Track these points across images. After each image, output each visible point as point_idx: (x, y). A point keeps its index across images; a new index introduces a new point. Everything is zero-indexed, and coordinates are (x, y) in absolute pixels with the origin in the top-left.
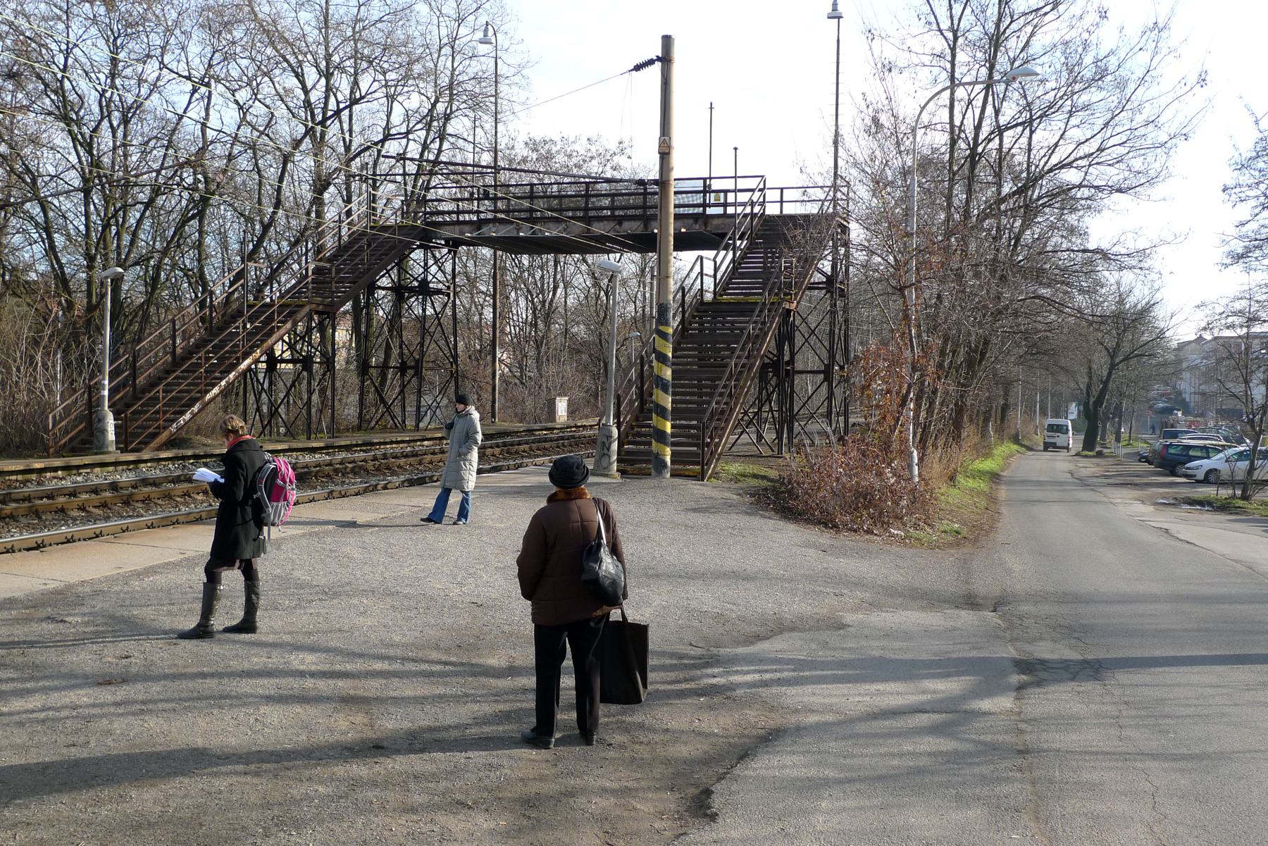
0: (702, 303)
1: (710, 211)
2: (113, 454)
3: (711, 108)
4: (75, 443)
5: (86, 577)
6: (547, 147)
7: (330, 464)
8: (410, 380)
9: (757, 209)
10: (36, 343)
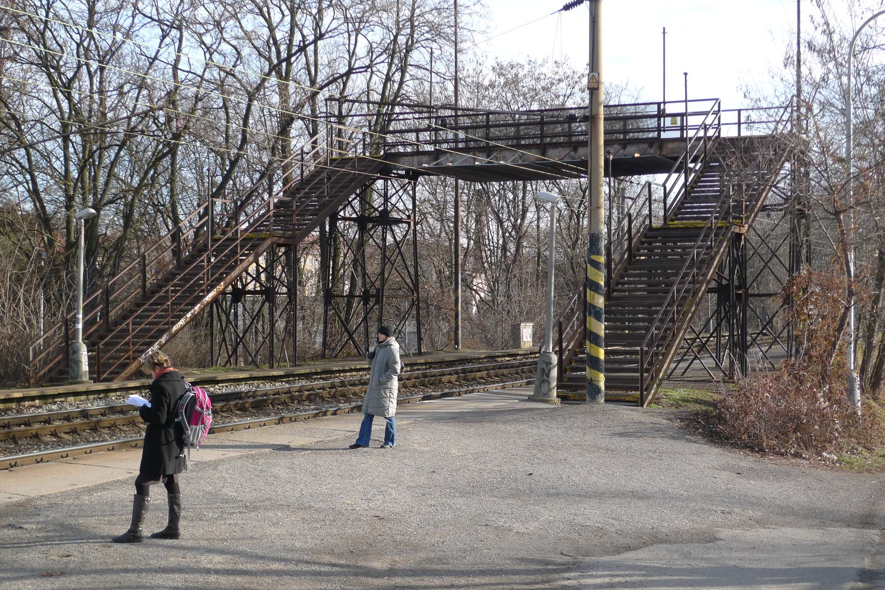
0: (650, 228)
1: (664, 135)
2: (86, 383)
3: (664, 33)
4: (53, 374)
5: (45, 492)
6: (514, 71)
7: (288, 392)
8: (372, 308)
9: (711, 132)
10: (19, 280)
